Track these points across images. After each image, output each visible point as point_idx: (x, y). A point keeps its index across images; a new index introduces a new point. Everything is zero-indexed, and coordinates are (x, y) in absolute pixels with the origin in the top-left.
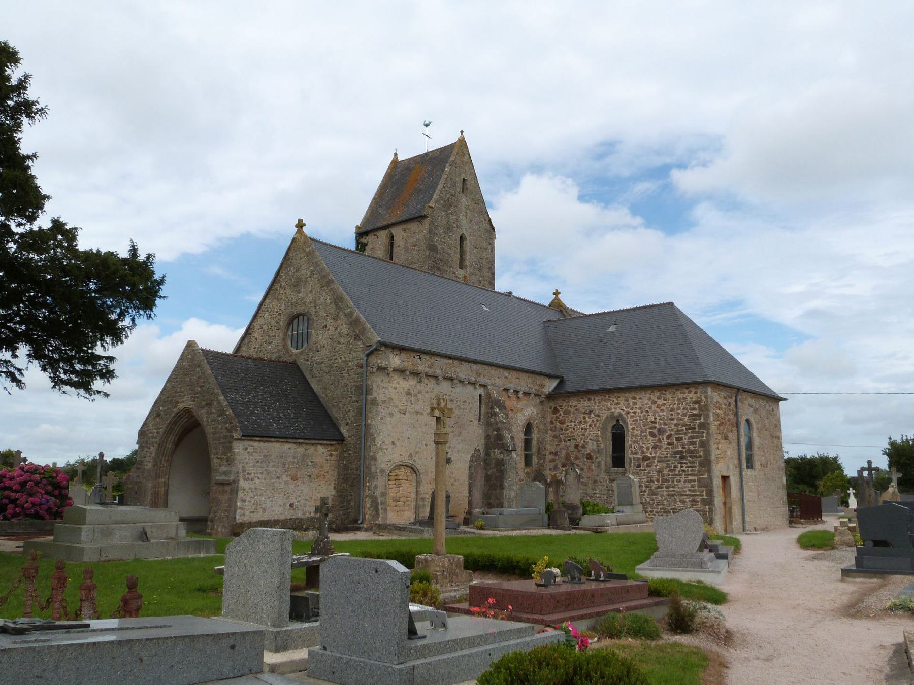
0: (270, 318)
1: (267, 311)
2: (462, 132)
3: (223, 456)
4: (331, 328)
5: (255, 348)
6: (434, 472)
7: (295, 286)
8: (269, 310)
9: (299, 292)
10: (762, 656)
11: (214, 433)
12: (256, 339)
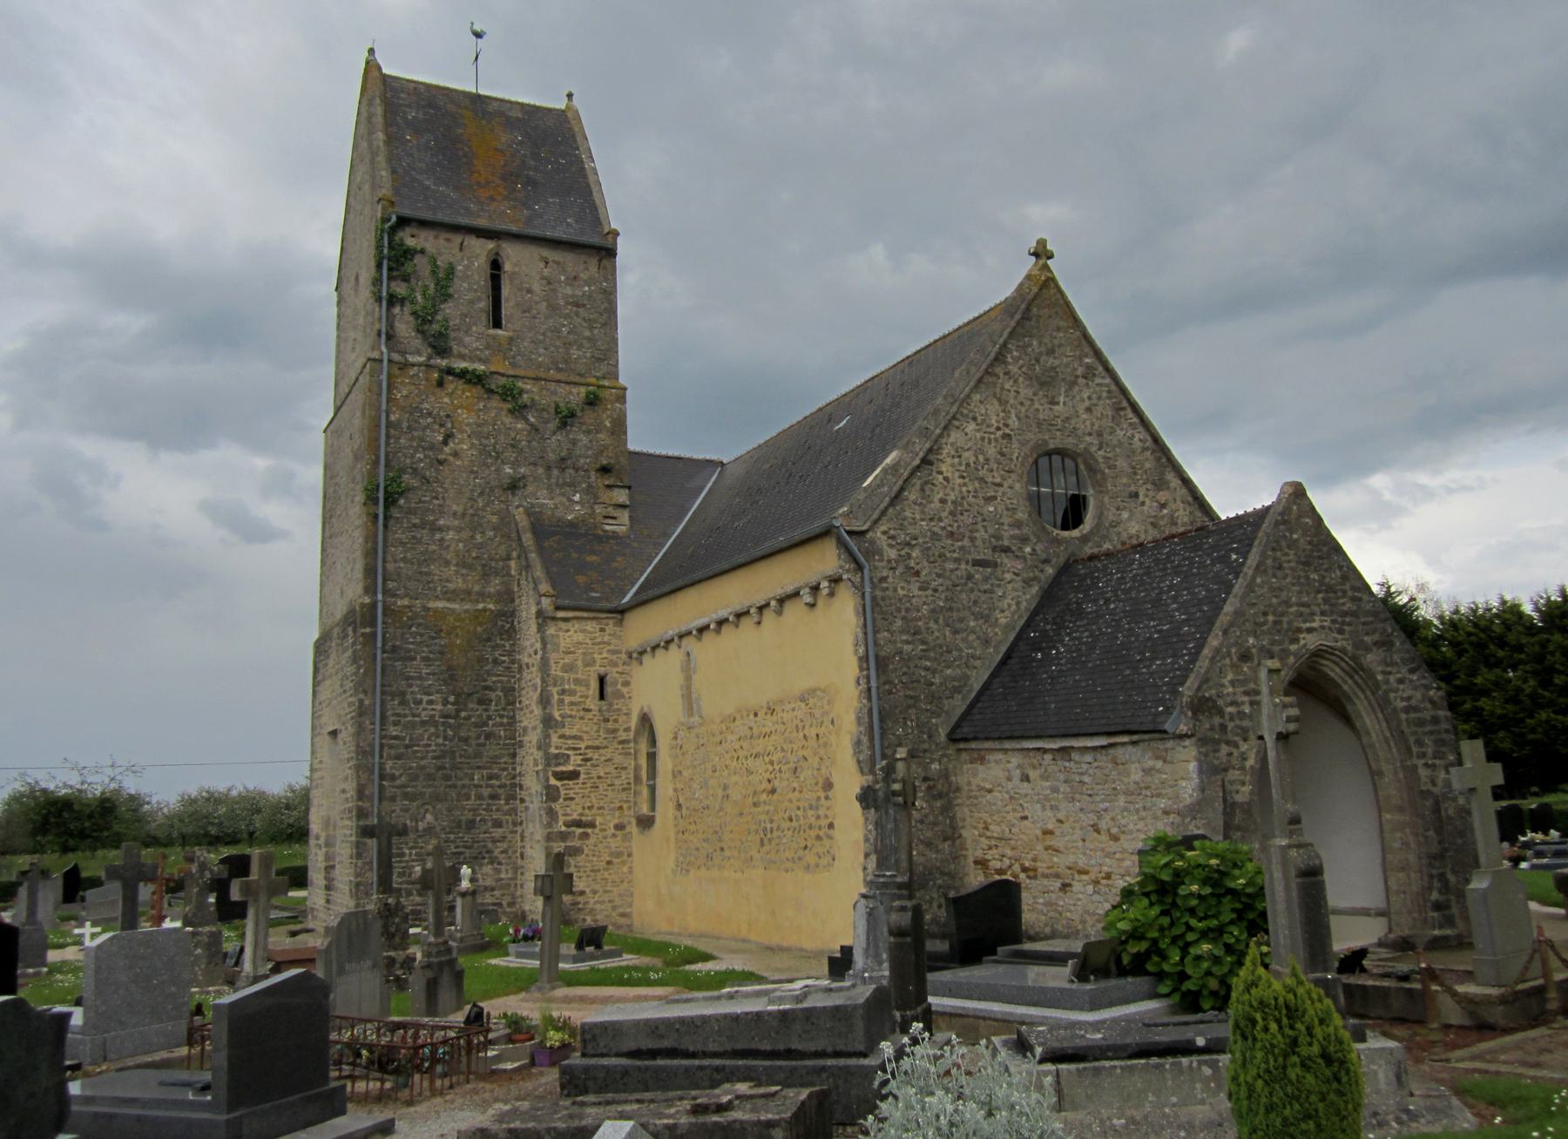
0: (983, 439)
1: (974, 419)
2: (570, 96)
3: (1437, 762)
4: (1148, 501)
5: (943, 501)
6: (396, 871)
7: (1042, 384)
8: (980, 418)
9: (1053, 402)
10: (651, 1128)
11: (1407, 710)
12: (946, 479)
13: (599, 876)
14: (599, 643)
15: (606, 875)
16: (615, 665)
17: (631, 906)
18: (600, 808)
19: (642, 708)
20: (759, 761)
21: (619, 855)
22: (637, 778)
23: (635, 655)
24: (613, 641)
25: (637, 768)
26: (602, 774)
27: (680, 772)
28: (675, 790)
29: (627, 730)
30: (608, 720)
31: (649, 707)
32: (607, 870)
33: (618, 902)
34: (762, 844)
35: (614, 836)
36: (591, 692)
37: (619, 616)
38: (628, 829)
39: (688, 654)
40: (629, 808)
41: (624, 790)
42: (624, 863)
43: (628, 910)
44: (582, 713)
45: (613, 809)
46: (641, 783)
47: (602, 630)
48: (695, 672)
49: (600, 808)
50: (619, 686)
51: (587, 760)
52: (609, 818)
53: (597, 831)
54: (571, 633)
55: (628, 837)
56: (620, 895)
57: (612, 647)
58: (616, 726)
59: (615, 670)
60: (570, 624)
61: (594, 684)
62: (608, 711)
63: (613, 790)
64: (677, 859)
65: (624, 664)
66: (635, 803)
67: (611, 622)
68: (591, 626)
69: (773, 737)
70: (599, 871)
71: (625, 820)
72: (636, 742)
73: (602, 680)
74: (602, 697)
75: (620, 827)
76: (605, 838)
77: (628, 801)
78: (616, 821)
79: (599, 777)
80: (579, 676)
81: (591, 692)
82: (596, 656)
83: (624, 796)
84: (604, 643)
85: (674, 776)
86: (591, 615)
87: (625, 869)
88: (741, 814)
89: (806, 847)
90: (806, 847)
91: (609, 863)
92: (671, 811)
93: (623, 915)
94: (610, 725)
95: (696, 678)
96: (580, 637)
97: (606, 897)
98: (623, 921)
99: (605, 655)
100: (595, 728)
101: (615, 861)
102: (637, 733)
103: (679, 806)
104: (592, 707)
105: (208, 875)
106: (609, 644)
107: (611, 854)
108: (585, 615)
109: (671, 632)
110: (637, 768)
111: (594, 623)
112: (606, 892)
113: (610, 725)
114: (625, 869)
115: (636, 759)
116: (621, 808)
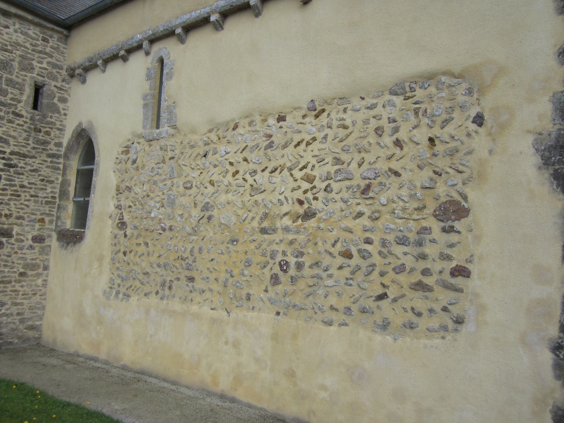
13: (9, 288)
14: (40, 52)
15: (18, 287)
16: (55, 79)
17: (41, 319)
18: (19, 218)
19: (80, 124)
20: (277, 178)
21: (34, 267)
22: (63, 194)
23: (78, 71)
24: (55, 55)
25: (65, 184)
26: (26, 183)
27: (129, 189)
28: (119, 207)
29: (59, 145)
30: (40, 131)
31: (91, 123)
32: (19, 281)
33: (27, 315)
34: (275, 280)
35: (31, 247)
36: (24, 98)
37: (65, 32)
38: (47, 242)
39: (161, 61)
40: (51, 222)
41: (47, 203)
42: (39, 275)
43: (38, 323)
44: (11, 116)
45: (34, 221)
46: (68, 199)
47: (44, 40)
48: (170, 77)
49: (19, 218)
50: (56, 101)
51: (11, 166)
52: (27, 229)
53: (12, 241)
54: (11, 30)
55: (45, 251)
56: (31, 308)
57: (54, 61)
58: (47, 138)
59: (54, 83)
60: (10, 22)
61: (29, 91)
62: (41, 121)
63: (36, 202)
64: (112, 280)
65: (63, 80)
66: (58, 218)
67: (56, 36)
68: (33, 31)
69: (316, 146)
70: (10, 282)
71: (45, 233)
72: (66, 157)
73: (38, 90)
74: (35, 106)
75: (39, 239)
76: (21, 249)
77: (49, 215)
78: (35, 233)
79: (22, 186)
80: (14, 77)
81: (24, 98)
82: (34, 63)
83: (47, 209)
84: (46, 53)
85: (119, 191)
86: (37, 20)
87: (40, 282)
88: (234, 241)
89: (382, 297)
90: (382, 297)
91: (22, 274)
92: (109, 227)
93: (32, 328)
94: (41, 136)
95: (170, 86)
96: (21, 39)
97: (14, 310)
98: (31, 333)
99: (45, 65)
100: (24, 135)
101: (30, 273)
102: (70, 149)
103: (122, 225)
104: (24, 113)
105: (314, 229)
106: (51, 57)
107: (26, 266)
108: (30, 17)
109: (139, 37)
110: (65, 184)
111: (37, 30)
112: (16, 304)
113: (41, 136)
114: (40, 282)
115: (64, 174)
116: (42, 221)
